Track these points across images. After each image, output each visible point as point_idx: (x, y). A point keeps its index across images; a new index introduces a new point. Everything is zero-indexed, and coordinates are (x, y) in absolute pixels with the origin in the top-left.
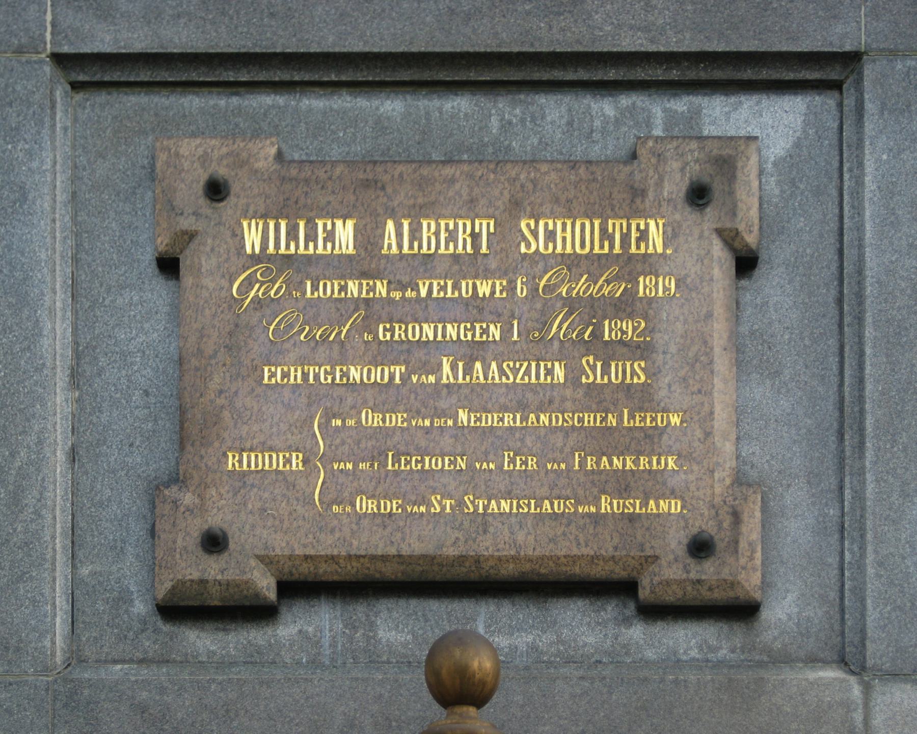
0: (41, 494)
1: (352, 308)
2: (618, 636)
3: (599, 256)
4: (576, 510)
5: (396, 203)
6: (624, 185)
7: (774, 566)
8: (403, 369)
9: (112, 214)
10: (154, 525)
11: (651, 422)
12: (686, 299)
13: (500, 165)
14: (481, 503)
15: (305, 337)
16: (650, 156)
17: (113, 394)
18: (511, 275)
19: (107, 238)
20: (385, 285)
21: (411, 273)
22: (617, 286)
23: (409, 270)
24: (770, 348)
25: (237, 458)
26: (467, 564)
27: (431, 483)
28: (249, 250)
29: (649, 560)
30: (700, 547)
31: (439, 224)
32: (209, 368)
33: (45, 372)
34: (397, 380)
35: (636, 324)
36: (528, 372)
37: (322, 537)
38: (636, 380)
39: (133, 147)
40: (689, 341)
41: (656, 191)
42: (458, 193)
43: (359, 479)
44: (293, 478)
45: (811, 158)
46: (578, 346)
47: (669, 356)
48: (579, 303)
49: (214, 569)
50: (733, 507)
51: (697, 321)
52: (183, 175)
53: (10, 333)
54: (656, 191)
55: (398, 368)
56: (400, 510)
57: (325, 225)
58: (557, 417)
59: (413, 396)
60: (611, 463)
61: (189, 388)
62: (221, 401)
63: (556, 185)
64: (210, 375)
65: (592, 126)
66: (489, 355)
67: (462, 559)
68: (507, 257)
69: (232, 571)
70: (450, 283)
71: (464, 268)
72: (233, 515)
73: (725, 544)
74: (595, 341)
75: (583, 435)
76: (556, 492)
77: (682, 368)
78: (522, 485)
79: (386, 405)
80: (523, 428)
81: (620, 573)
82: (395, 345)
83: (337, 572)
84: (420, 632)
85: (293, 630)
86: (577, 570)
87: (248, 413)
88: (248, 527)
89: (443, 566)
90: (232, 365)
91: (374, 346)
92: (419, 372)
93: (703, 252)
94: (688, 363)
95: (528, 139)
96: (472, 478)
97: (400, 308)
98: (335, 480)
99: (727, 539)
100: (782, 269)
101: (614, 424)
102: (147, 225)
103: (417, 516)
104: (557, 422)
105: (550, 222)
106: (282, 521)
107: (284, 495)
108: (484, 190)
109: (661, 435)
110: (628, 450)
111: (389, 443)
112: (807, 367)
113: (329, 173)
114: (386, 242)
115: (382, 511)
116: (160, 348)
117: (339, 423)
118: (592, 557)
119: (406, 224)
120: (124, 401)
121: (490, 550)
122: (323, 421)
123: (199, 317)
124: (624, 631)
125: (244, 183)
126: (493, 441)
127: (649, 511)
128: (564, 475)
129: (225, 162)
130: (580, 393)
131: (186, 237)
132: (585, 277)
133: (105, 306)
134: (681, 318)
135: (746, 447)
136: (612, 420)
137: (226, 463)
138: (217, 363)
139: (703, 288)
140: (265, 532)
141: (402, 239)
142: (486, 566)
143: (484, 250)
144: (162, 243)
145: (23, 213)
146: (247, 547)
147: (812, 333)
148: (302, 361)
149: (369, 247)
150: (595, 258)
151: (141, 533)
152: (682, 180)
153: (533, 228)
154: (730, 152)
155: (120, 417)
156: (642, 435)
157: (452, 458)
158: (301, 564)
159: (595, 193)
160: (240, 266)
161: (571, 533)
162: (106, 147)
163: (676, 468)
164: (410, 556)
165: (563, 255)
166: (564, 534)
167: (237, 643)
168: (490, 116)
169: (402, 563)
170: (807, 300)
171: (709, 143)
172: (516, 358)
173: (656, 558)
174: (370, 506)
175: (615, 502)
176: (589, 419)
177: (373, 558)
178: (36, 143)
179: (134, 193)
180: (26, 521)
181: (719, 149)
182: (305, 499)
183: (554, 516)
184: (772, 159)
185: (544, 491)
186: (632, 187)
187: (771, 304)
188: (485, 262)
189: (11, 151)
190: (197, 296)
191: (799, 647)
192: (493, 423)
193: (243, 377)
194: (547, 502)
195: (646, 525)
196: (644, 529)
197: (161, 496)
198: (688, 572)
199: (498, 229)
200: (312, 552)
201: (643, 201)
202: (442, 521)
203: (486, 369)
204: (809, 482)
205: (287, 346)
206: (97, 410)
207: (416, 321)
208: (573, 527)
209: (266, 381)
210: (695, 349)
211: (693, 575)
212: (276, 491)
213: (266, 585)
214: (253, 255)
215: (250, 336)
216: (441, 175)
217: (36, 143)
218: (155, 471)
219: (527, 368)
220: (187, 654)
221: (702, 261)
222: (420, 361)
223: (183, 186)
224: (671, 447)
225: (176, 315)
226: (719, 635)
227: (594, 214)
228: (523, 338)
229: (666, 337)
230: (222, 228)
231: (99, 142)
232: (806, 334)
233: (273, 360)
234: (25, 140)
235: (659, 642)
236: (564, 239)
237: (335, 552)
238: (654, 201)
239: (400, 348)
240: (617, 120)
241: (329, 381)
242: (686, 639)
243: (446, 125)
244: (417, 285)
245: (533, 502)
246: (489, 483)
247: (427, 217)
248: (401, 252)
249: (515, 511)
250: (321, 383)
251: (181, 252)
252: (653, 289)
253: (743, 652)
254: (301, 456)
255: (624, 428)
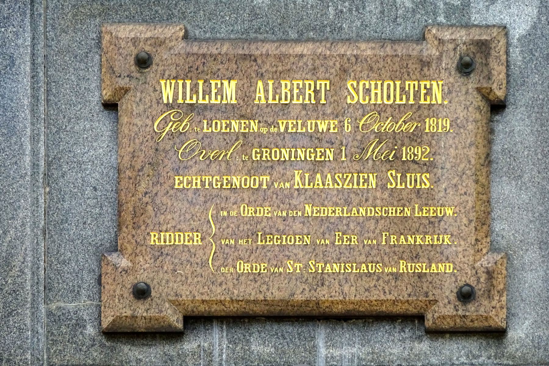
0: (24, 259)
1: (234, 139)
2: (412, 348)
3: (399, 105)
4: (383, 270)
5: (264, 70)
6: (416, 59)
7: (517, 303)
8: (268, 178)
9: (71, 70)
10: (100, 276)
11: (433, 214)
12: (457, 134)
13: (333, 45)
14: (320, 265)
15: (203, 158)
16: (434, 39)
17: (72, 189)
18: (340, 117)
19: (68, 86)
20: (257, 124)
21: (274, 116)
22: (411, 125)
23: (273, 114)
24: (515, 160)
25: (157, 237)
26: (311, 306)
27: (287, 253)
28: (165, 101)
29: (432, 302)
30: (466, 296)
31: (293, 84)
32: (138, 178)
33: (27, 179)
34: (265, 187)
35: (424, 150)
36: (351, 181)
37: (214, 288)
38: (423, 186)
39: (86, 26)
40: (458, 161)
41: (437, 63)
42: (305, 64)
43: (238, 251)
44: (194, 250)
45: (543, 36)
46: (385, 164)
47: (445, 170)
48: (386, 136)
49: (142, 309)
50: (487, 268)
51: (464, 148)
52: (121, 50)
53: (3, 153)
54: (437, 63)
55: (265, 178)
56: (266, 271)
57: (216, 84)
58: (371, 210)
59: (275, 196)
60: (406, 240)
61: (124, 190)
62: (146, 199)
63: (371, 59)
64: (139, 182)
65: (397, 14)
66: (326, 170)
67: (307, 302)
68: (338, 106)
69: (153, 310)
70: (300, 122)
71: (309, 113)
72: (154, 273)
73: (482, 292)
74: (396, 161)
75: (388, 221)
76: (370, 258)
77: (454, 178)
78: (348, 254)
79: (257, 203)
80: (348, 217)
81: (412, 310)
82: (263, 163)
83: (223, 310)
84: (280, 346)
85: (194, 345)
86: (384, 308)
87: (165, 207)
88: (164, 281)
89: (295, 306)
90: (154, 175)
91: (249, 164)
92: (279, 181)
93: (468, 103)
94: (458, 175)
95: (354, 22)
96: (314, 249)
97: (266, 139)
98: (222, 251)
99: (483, 289)
100: (523, 109)
101: (409, 215)
102: (95, 78)
103: (277, 275)
104: (371, 213)
105: (367, 83)
106: (187, 278)
107: (188, 261)
108: (322, 62)
109: (440, 221)
110: (418, 231)
111: (258, 227)
112: (539, 173)
113: (220, 50)
114: (258, 95)
115: (254, 271)
116: (104, 159)
117: (225, 214)
118: (394, 300)
119: (271, 83)
120: (79, 194)
121: (326, 296)
122: (215, 212)
123: (132, 144)
124: (417, 345)
125: (162, 57)
126: (328, 226)
127: (432, 271)
128: (376, 247)
129: (149, 42)
130: (386, 195)
131: (123, 91)
132: (390, 118)
133: (67, 131)
134: (454, 146)
135: (498, 225)
136: (408, 212)
137: (150, 240)
138: (143, 175)
139: (468, 126)
140: (176, 285)
141: (268, 94)
142: (323, 306)
143: (323, 101)
144: (106, 94)
145: (12, 73)
146: (163, 294)
147: (543, 151)
148: (200, 172)
149: (246, 99)
150: (397, 106)
151: (92, 282)
152: (454, 56)
153: (355, 87)
154: (487, 38)
155: (77, 205)
156: (427, 221)
157: (301, 237)
158: (199, 306)
159: (397, 64)
160: (159, 111)
161: (380, 286)
162: (68, 26)
163: (450, 243)
164: (273, 301)
165: (375, 105)
166: (375, 286)
167: (156, 353)
168: (328, 7)
169: (267, 305)
170: (540, 129)
171: (473, 30)
172: (344, 171)
173: (436, 301)
174: (246, 268)
175: (409, 265)
176: (392, 212)
177: (248, 302)
178: (21, 27)
179: (87, 56)
180: (14, 276)
181: (480, 35)
182: (202, 264)
183: (369, 275)
184: (517, 36)
185: (363, 258)
186: (421, 61)
187: (515, 131)
188: (323, 109)
189: (4, 33)
190: (130, 130)
191: (533, 355)
192: (328, 214)
193: (161, 184)
194: (364, 265)
195: (430, 280)
196: (428, 283)
197: (106, 260)
198: (457, 310)
199: (332, 87)
200: (207, 298)
201: (429, 70)
202: (294, 278)
203: (324, 177)
204: (540, 248)
205: (190, 163)
206: (61, 200)
207: (277, 147)
208: (381, 282)
209: (176, 186)
210: (462, 166)
211: (460, 313)
212: (183, 258)
213: (176, 320)
214: (167, 105)
215: (166, 156)
216: (294, 52)
217: (21, 27)
218: (101, 240)
219: (351, 178)
220: (122, 361)
221: (467, 109)
222: (280, 173)
223: (121, 58)
224: (446, 229)
225: (116, 134)
226: (480, 348)
227: (396, 78)
228: (349, 158)
229: (443, 158)
230: (147, 86)
231: (63, 22)
232: (539, 151)
233: (181, 173)
234: (13, 25)
235: (440, 353)
236: (376, 94)
237: (223, 298)
238: (436, 69)
239: (266, 165)
240: (414, 11)
241: (219, 186)
242: (456, 350)
243: (299, 13)
244: (278, 124)
245: (354, 265)
246: (326, 253)
247: (285, 79)
248: (267, 102)
249: (342, 271)
250: (213, 188)
251: (119, 100)
252: (435, 127)
253: (496, 359)
254: (200, 235)
255: (415, 217)
